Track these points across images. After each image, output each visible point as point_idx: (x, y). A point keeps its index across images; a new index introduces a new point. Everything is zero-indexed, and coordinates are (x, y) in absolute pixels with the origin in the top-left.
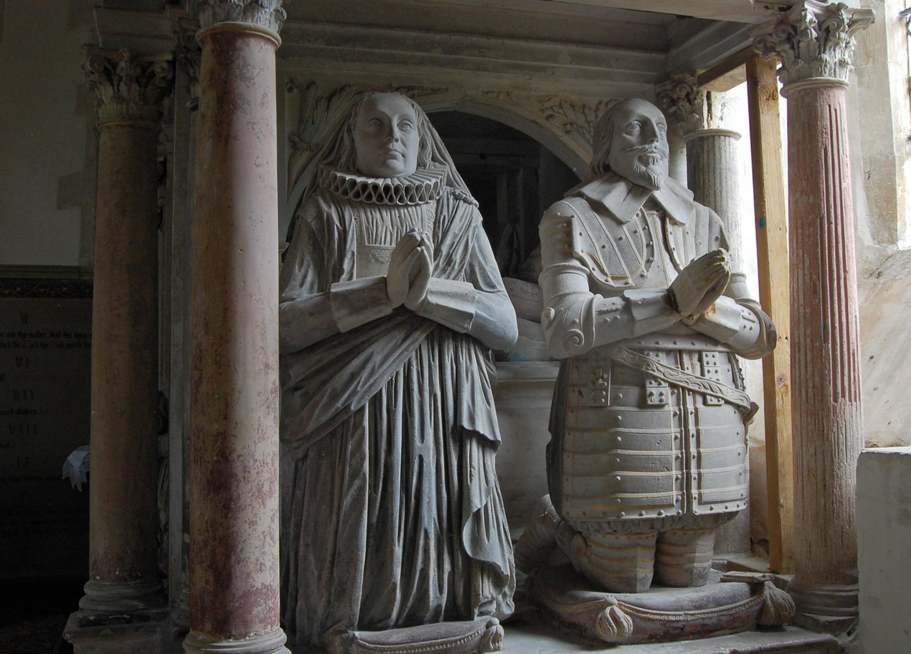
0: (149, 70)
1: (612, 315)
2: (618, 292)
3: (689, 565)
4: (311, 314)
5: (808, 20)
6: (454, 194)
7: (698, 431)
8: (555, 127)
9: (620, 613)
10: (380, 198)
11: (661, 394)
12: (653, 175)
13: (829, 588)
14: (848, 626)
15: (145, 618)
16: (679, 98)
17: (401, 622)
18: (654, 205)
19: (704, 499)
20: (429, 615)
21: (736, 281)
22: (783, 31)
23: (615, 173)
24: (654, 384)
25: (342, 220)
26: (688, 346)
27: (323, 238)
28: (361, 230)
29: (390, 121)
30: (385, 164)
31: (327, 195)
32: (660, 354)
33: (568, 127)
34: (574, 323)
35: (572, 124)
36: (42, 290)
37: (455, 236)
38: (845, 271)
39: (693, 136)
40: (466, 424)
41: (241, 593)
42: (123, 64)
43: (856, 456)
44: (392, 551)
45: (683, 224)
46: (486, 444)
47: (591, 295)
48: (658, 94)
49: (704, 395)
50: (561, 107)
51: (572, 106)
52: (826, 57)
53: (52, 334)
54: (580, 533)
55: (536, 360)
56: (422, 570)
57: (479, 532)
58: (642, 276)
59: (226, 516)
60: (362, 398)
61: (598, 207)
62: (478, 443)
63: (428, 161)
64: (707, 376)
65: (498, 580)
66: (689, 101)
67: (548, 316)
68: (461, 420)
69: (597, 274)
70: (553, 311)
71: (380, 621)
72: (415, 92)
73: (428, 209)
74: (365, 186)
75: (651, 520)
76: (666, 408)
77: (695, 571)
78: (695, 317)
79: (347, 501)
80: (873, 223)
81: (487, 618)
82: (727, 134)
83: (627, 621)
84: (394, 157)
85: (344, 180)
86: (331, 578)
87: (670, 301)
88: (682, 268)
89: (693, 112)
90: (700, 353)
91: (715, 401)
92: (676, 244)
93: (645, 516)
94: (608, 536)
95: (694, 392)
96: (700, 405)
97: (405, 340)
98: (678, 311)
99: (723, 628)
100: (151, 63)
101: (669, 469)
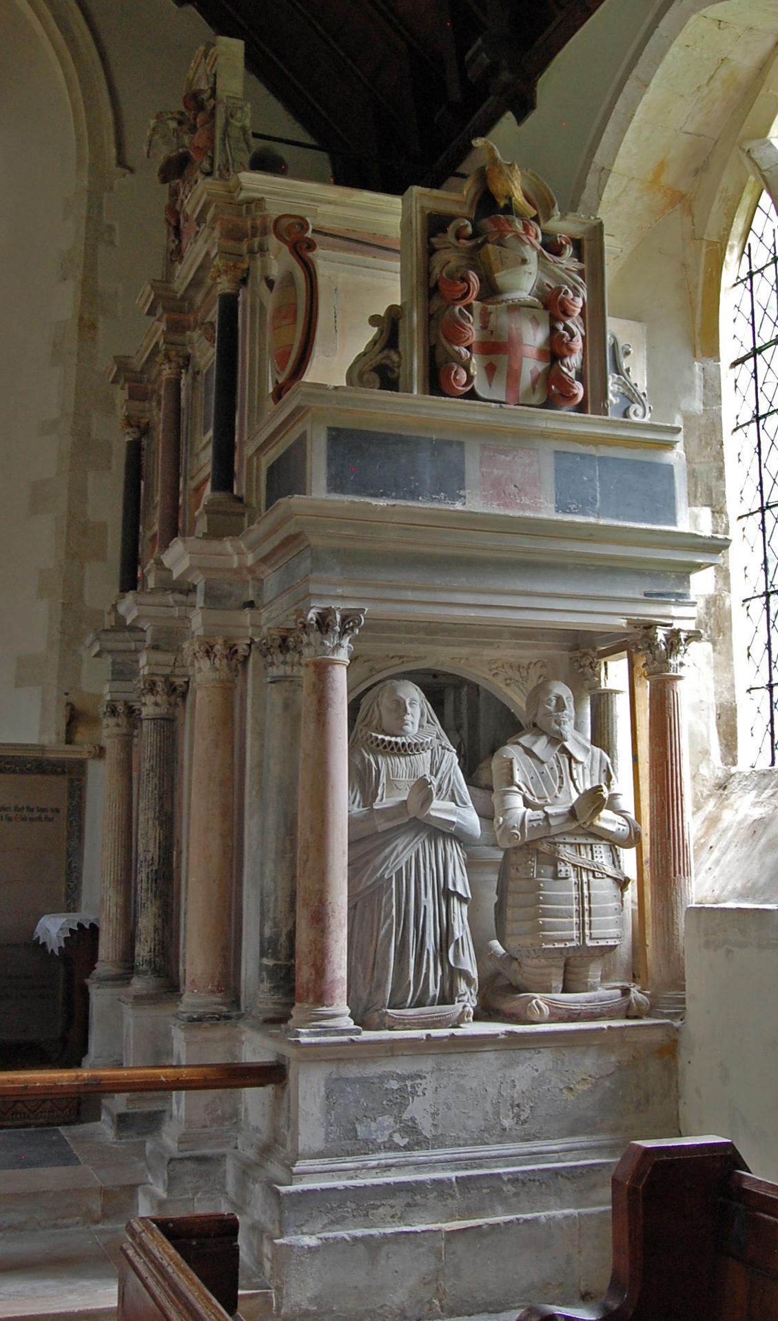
0: (235, 648)
1: (538, 822)
2: (541, 807)
3: (585, 980)
4: (362, 821)
5: (658, 640)
6: (441, 745)
7: (589, 894)
8: (499, 682)
9: (541, 1003)
10: (399, 750)
11: (567, 871)
12: (564, 733)
13: (671, 993)
14: (679, 1015)
15: (228, 1018)
16: (585, 665)
17: (413, 1004)
18: (565, 750)
19: (593, 936)
20: (429, 1001)
21: (617, 798)
22: (646, 642)
23: (540, 730)
24: (563, 864)
25: (377, 763)
26: (584, 841)
27: (365, 774)
28: (388, 770)
29: (405, 702)
30: (402, 729)
31: (367, 748)
32: (567, 846)
33: (508, 681)
34: (514, 827)
35: (511, 679)
36: (8, 766)
37: (443, 772)
38: (682, 795)
39: (593, 692)
40: (451, 888)
41: (330, 980)
42: (218, 647)
43: (684, 910)
44: (408, 962)
45: (582, 763)
46: (462, 899)
47: (525, 809)
48: (571, 659)
49: (593, 872)
50: (503, 667)
51: (511, 667)
52: (671, 661)
53: (16, 808)
54: (516, 959)
55: (483, 845)
56: (426, 974)
57: (458, 952)
58: (556, 797)
59: (322, 937)
60: (391, 871)
61: (529, 752)
62: (458, 899)
63: (425, 724)
64: (596, 860)
65: (469, 982)
66: (592, 668)
67: (498, 822)
68: (448, 885)
69: (528, 795)
70: (501, 819)
71: (402, 1003)
72: (405, 659)
73: (426, 756)
74: (390, 742)
75: (561, 948)
76: (570, 879)
77: (589, 984)
78: (588, 823)
79: (382, 932)
80: (721, 750)
81: (462, 1004)
82: (617, 692)
83: (546, 1009)
84: (407, 724)
85: (377, 738)
86: (372, 979)
87: (572, 814)
88: (581, 792)
89: (594, 675)
90: (591, 845)
91: (600, 875)
92: (578, 775)
93: (557, 946)
94: (534, 960)
95: (588, 870)
96: (591, 878)
97: (416, 836)
98: (577, 820)
99: (604, 1016)
100: (235, 645)
101: (572, 917)
